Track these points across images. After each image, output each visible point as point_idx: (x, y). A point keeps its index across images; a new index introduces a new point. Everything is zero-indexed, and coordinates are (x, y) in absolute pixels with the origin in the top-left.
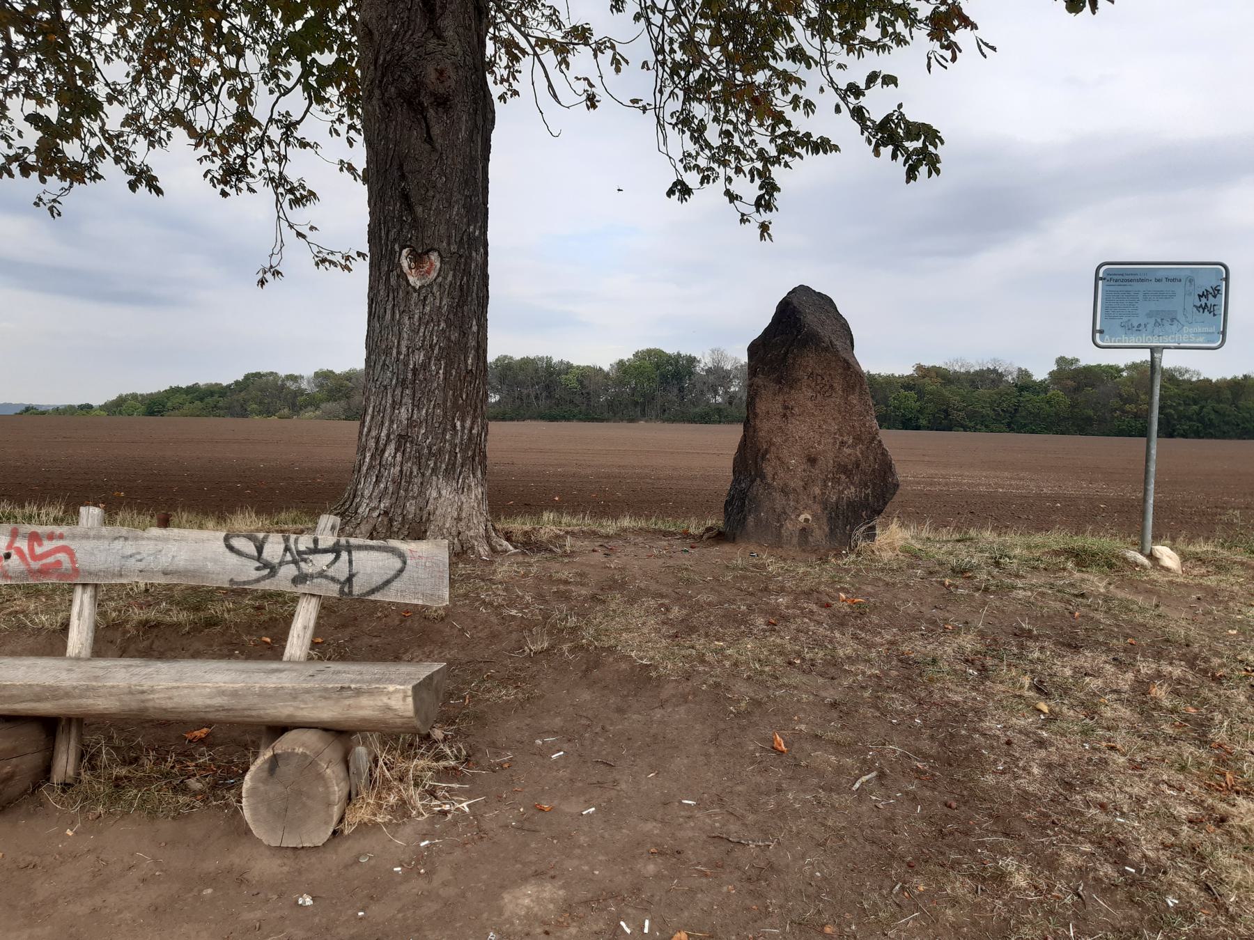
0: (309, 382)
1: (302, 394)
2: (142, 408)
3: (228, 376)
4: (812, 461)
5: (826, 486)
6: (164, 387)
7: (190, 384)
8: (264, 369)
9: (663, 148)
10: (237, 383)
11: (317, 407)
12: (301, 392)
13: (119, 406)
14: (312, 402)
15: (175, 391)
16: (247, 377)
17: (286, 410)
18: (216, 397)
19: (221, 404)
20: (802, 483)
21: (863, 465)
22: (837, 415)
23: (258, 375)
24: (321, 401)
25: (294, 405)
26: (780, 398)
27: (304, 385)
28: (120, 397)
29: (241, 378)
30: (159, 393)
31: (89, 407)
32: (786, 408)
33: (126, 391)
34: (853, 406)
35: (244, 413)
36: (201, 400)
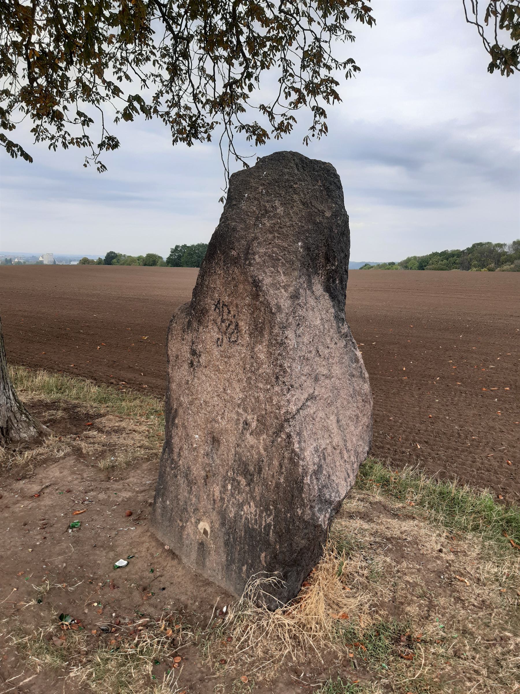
0: (509, 247)
1: (504, 255)
2: (417, 264)
3: (463, 245)
4: (215, 441)
5: (224, 487)
6: (429, 253)
7: (443, 250)
8: (484, 241)
9: (472, 17)
10: (468, 249)
11: (512, 263)
12: (505, 253)
13: (406, 264)
14: (510, 259)
15: (435, 254)
16: (474, 246)
17: (493, 265)
18: (455, 257)
19: (457, 261)
20: (203, 473)
21: (266, 472)
22: (242, 376)
23: (481, 244)
24: (516, 259)
25: (499, 261)
26: (189, 337)
27: (506, 249)
28: (408, 258)
29: (470, 246)
30: (427, 256)
31: (393, 264)
32: (194, 353)
33: (411, 255)
34: (260, 365)
35: (468, 268)
36: (447, 259)
